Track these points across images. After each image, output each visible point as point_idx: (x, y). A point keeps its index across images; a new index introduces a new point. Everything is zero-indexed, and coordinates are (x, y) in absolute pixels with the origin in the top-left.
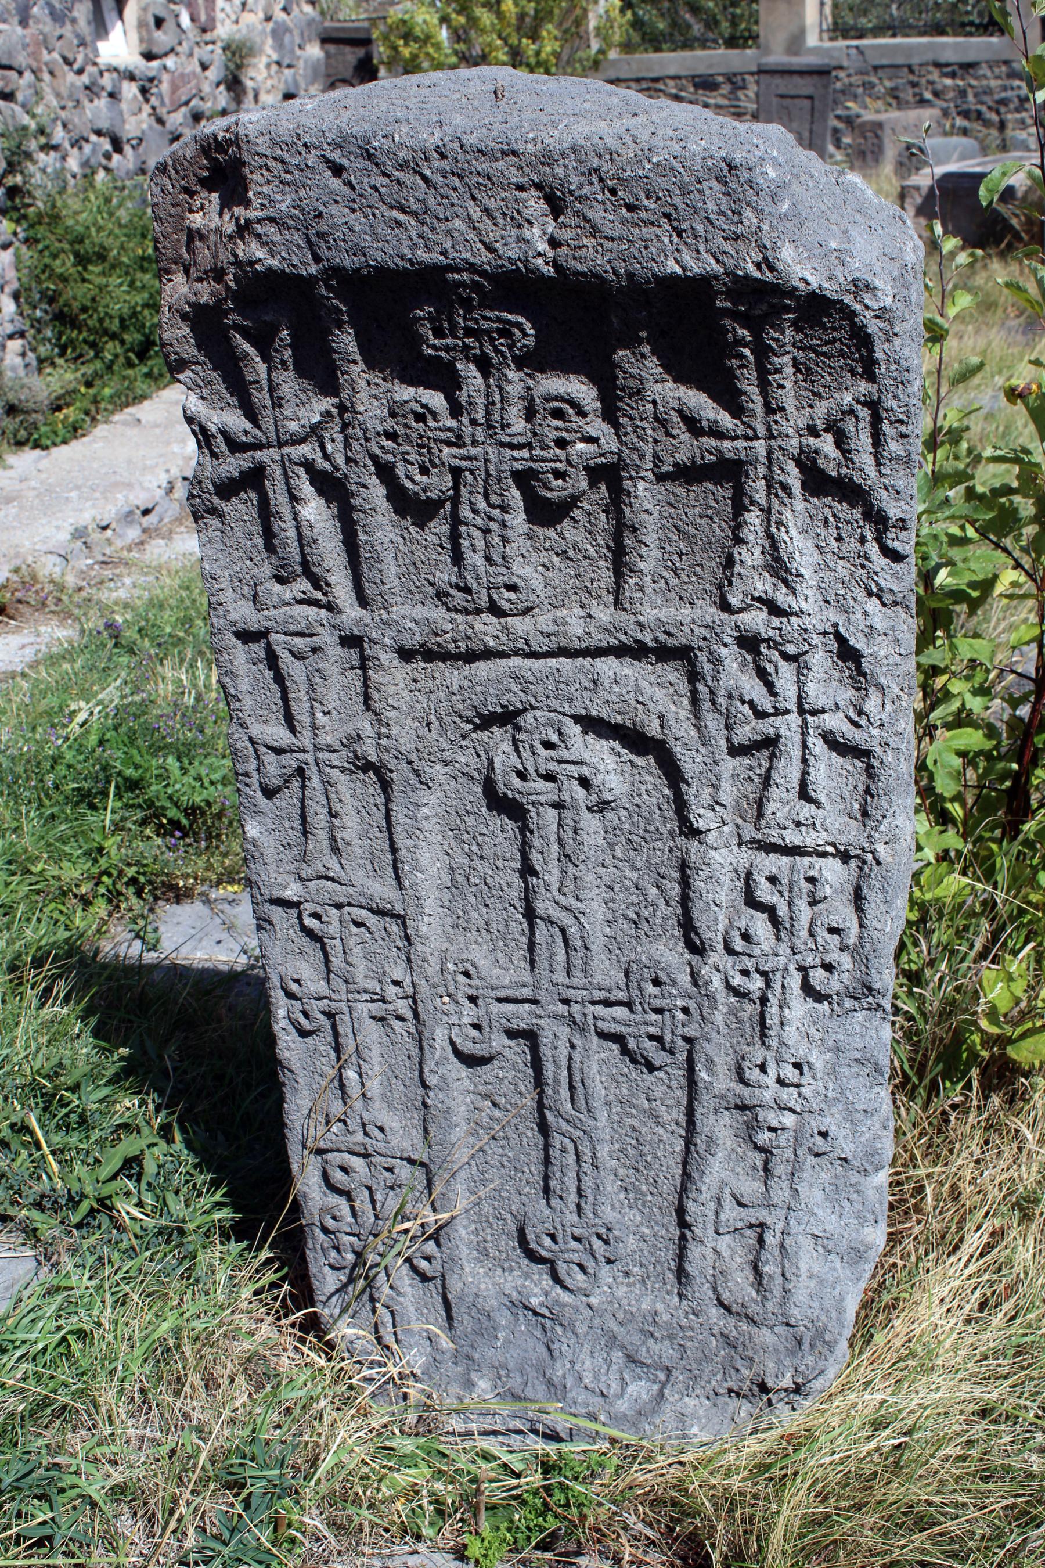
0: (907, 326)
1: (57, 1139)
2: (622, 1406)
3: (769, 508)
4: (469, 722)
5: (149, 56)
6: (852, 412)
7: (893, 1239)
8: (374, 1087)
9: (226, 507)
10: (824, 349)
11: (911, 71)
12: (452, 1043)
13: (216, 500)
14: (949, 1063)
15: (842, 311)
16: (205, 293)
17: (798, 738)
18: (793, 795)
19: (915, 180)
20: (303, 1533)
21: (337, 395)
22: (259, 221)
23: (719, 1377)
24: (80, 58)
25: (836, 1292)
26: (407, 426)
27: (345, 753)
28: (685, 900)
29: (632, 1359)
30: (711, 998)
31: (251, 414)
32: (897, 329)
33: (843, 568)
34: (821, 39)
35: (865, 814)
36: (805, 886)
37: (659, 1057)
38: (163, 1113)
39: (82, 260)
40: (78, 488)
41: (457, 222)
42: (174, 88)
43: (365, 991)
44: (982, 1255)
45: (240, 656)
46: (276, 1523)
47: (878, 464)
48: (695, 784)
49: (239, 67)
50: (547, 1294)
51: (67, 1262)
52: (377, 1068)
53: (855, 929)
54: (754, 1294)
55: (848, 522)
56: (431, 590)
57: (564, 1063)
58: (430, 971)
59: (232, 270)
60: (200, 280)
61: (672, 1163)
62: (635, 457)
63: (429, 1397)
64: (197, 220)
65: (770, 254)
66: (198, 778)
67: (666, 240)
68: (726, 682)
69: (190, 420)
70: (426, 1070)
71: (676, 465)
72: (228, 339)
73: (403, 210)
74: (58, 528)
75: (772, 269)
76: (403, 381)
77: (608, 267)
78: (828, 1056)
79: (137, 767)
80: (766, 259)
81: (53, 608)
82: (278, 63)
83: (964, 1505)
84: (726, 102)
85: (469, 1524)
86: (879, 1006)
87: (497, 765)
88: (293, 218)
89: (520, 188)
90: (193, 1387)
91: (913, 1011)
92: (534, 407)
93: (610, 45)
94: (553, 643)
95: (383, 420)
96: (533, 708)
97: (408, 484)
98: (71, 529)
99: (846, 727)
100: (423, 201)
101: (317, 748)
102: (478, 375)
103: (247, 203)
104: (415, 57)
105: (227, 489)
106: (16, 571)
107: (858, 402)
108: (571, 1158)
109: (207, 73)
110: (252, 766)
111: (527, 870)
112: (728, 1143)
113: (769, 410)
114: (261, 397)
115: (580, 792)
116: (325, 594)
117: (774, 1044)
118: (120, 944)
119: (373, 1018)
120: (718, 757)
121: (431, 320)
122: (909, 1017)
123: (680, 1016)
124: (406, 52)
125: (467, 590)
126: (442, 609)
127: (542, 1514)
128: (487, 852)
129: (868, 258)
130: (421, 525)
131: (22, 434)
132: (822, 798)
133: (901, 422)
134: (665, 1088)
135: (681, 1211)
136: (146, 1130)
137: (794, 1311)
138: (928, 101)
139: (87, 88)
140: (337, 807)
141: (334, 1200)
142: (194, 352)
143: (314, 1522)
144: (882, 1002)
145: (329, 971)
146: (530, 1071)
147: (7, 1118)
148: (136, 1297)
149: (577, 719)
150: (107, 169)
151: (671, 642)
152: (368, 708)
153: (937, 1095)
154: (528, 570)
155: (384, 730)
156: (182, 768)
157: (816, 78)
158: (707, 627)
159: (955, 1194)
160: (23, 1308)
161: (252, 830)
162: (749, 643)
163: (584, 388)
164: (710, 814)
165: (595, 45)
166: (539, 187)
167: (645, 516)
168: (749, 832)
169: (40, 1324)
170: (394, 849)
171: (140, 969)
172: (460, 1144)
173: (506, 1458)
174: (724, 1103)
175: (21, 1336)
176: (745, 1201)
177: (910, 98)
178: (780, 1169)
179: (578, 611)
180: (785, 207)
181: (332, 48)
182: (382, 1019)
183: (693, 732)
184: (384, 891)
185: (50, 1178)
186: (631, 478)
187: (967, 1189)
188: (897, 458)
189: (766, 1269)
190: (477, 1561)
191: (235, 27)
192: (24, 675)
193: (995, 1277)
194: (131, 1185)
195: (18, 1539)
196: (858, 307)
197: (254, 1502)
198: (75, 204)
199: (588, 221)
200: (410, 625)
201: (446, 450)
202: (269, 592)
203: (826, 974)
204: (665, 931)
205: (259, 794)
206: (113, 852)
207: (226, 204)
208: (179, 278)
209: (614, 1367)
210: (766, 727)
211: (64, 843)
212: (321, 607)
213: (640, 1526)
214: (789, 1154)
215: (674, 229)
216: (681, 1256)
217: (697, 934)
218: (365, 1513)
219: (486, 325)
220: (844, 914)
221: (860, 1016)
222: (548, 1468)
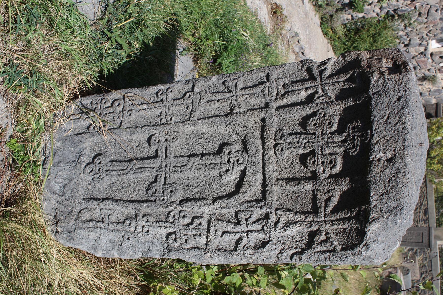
0: (357, 260)
1: (127, 26)
2: (52, 183)
3: (305, 222)
4: (244, 138)
5: (432, 54)
6: (332, 244)
7: (99, 259)
8: (142, 113)
9: (304, 70)
10: (350, 237)
11: (430, 271)
12: (154, 135)
13: (306, 67)
14: (149, 273)
15: (361, 241)
16: (364, 63)
17: (240, 230)
18: (224, 229)
19: (399, 271)
20: (17, 93)
21: (336, 100)
22: (384, 78)
23: (60, 210)
24: (431, 35)
25: (84, 243)
26: (327, 120)
27: (235, 104)
28: (194, 199)
29: (65, 185)
30: (167, 207)
31: (330, 77)
32: (356, 257)
33: (288, 243)
34: (439, 245)
35: (219, 250)
36: (199, 233)
37: (150, 192)
38: (134, 55)
39: (373, 36)
40: (310, 34)
41: (384, 133)
42: (423, 62)
43: (169, 110)
44: (94, 285)
45: (262, 75)
46: (20, 86)
47: (317, 252)
48: (227, 202)
49: (429, 80)
50: (84, 162)
51: (92, 29)
52: (147, 114)
53: (186, 247)
54: (84, 220)
55: (301, 244)
56: (281, 127)
57: (149, 166)
58: (174, 128)
59: (371, 70)
60: (368, 62)
61: (121, 196)
62: (319, 184)
63: (55, 129)
64: (384, 61)
65: (377, 220)
66: (228, 67)
67: (380, 191)
68: (256, 210)
69: (328, 59)
70: (147, 127)
71: (317, 195)
72: (351, 70)
73: (388, 118)
74: (298, 28)
75: (372, 221)
76: (340, 119)
77: (372, 175)
78: (151, 240)
79: (231, 50)
80: (375, 219)
81: (276, 27)
82: (430, 91)
83: (24, 278)
84: (421, 218)
85: (20, 140)
86: (165, 254)
87: (232, 146)
88: (385, 87)
89: (394, 150)
90: (58, 63)
91: (162, 266)
92: (333, 155)
93: (436, 185)
94: (266, 162)
95: (329, 113)
96: (248, 156)
97: (311, 120)
98: (298, 32)
99: (243, 244)
100: (390, 123)
101: (237, 96)
102: (342, 139)
103: (389, 74)
104: (433, 130)
105: (309, 70)
106: (286, 17)
107: (335, 246)
108: (122, 168)
109: (427, 71)
110: (232, 78)
111: (203, 155)
112: (126, 212)
113: (332, 221)
114: (335, 79)
115: (225, 169)
116: (280, 98)
117: (154, 225)
118: (182, 44)
119: (161, 113)
120: (235, 208)
121: (357, 126)
122: (161, 265)
123: (162, 198)
124: (434, 127)
125: (281, 137)
126: (276, 130)
127: (22, 160)
128: (208, 144)
129: (376, 248)
130: (299, 124)
131: (325, 19)
132: (223, 238)
133: (330, 258)
134: (141, 194)
135: (107, 199)
136: (130, 50)
137: (79, 231)
138: (422, 276)
139: (422, 37)
140: (220, 102)
141: (111, 102)
142: (348, 60)
143: (21, 96)
144: (166, 255)
145: (174, 100)
146: (146, 156)
147: (133, 12)
148: (83, 47)
149: (245, 168)
150: (400, 43)
151: (267, 194)
152: (248, 110)
153: (139, 273)
154: (287, 154)
155: (242, 114)
156: (231, 62)
157: (428, 243)
158: (271, 205)
159: (112, 278)
160: (80, 16)
161: (214, 78)
162: (267, 216)
163: (338, 169)
164: (219, 206)
165: (436, 181)
166: (395, 155)
167: (302, 187)
168: (214, 217)
169: (76, 21)
170: (208, 118)
171: (174, 49)
172: (125, 137)
173: (38, 150)
174: (137, 211)
175: (73, 15)
176: (110, 217)
177: (422, 271)
178: (119, 227)
179: (275, 168)
180: (390, 225)
181: (435, 106)
182: (161, 115)
183: (242, 201)
184: (197, 115)
185: (116, 24)
186: (313, 183)
187: (113, 281)
188: (319, 258)
189: (91, 223)
190: (9, 142)
191: (440, 79)
192: (257, 19)
193: (88, 288)
194: (114, 46)
195: (16, 14)
196: (362, 246)
197: (26, 80)
198: (389, 34)
199: (385, 169)
200: (271, 121)
201: (320, 131)
202: (280, 82)
203: (174, 239)
204: (186, 194)
205: (224, 80)
206: (208, 43)
207: (389, 69)
208: (368, 56)
209: (63, 181)
210: (243, 221)
211: (210, 29)
212: (276, 97)
213: (19, 188)
214: (123, 229)
215: (383, 194)
216: (94, 199)
217: (185, 203)
218: (23, 111)
219: (356, 141)
220: (191, 244)
221: (162, 249)
222: (35, 162)
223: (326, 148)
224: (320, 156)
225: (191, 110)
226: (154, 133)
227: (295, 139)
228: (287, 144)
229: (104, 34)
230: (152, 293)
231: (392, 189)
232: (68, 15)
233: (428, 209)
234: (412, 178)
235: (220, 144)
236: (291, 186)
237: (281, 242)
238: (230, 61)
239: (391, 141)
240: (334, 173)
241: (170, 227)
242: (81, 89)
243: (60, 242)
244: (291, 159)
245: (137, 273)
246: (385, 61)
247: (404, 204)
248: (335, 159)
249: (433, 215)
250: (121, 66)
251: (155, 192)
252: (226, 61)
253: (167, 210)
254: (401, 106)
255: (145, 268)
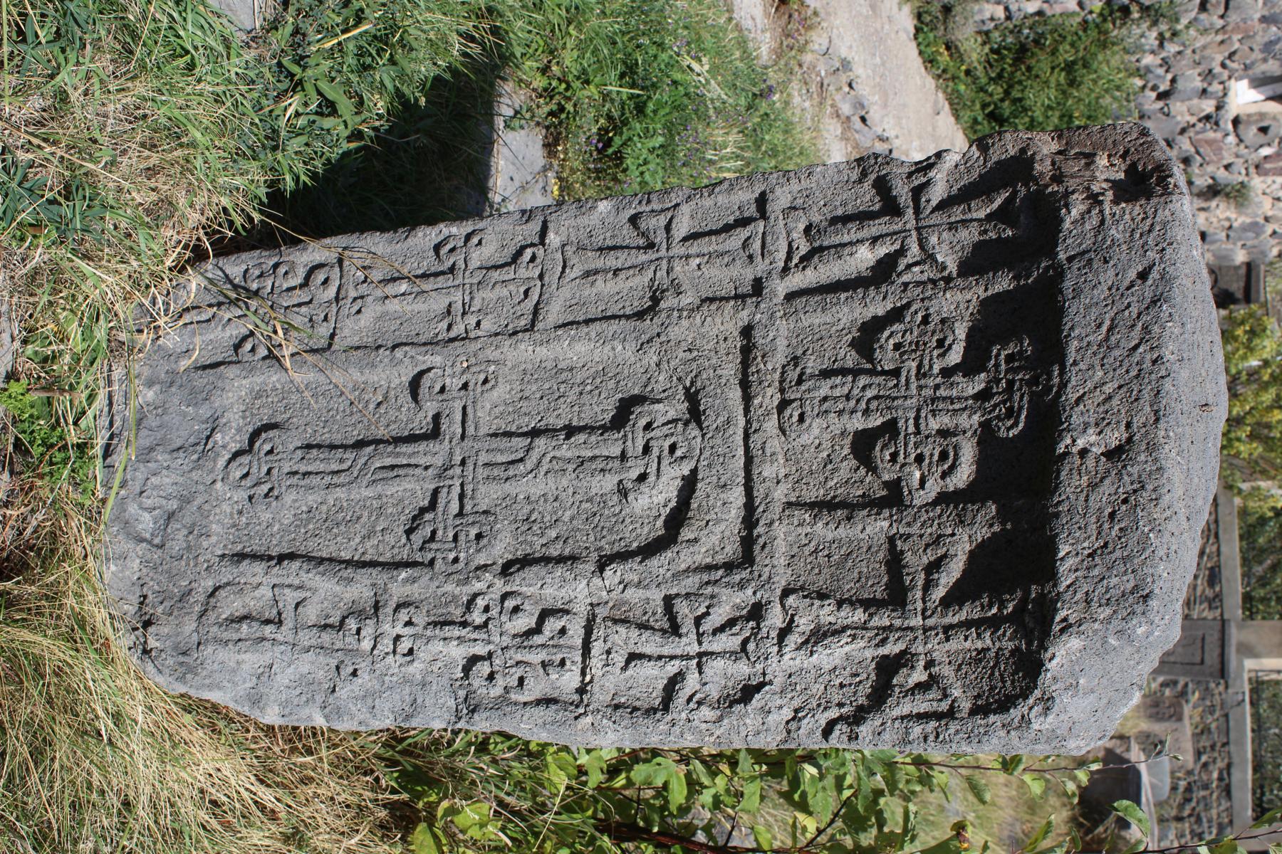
0: (1016, 742)
1: (351, 46)
2: (133, 509)
3: (866, 629)
4: (692, 383)
5: (1236, 122)
6: (945, 696)
7: (269, 730)
8: (394, 306)
10: (997, 674)
11: (1224, 745)
12: (429, 370)
13: (873, 176)
14: (412, 776)
15: (1028, 688)
16: (1043, 168)
17: (679, 652)
18: (632, 648)
20: (29, 248)
21: (959, 275)
22: (1101, 211)
23: (156, 588)
25: (225, 683)
26: (934, 332)
27: (666, 282)
28: (546, 560)
29: (171, 516)
30: (466, 581)
31: (943, 205)
32: (1013, 733)
33: (817, 689)
34: (1250, 671)
35: (617, 707)
36: (558, 658)
37: (417, 538)
38: (372, 133)
39: (1069, 67)
40: (883, 64)
41: (1100, 374)
42: (1210, 143)
43: (472, 299)
45: (745, 197)
46: (37, 226)
47: (903, 718)
48: (641, 568)
49: (1227, 195)
50: (224, 447)
51: (250, 55)
52: (409, 308)
54: (224, 616)
55: (855, 693)
56: (799, 353)
57: (413, 461)
58: (488, 352)
59: (1062, 189)
60: (1053, 163)
61: (331, 549)
62: (909, 519)
64: (1102, 161)
65: (1074, 629)
66: (646, 162)
67: (1086, 544)
68: (724, 593)
69: (939, 155)
70: (407, 348)
71: (902, 552)
72: (1005, 187)
73: (1110, 329)
74: (851, 47)
75: (1062, 631)
77: (1063, 497)
78: (419, 677)
79: (655, 112)
80: (1070, 626)
81: (785, 43)
82: (1230, 227)
83: (52, 788)
84: (1198, 593)
86: (460, 718)
87: (656, 406)
89: (1128, 425)
90: (149, 157)
92: (950, 437)
93: (1245, 498)
95: (939, 313)
96: (703, 436)
97: (886, 333)
98: (849, 58)
99: (687, 692)
100: (1117, 346)
101: (670, 259)
102: (975, 391)
103: (1116, 202)
104: (1236, 339)
105: (882, 186)
106: (816, 13)
107: (953, 701)
108: (335, 467)
109: (1222, 169)
110: (656, 205)
111: (570, 431)
112: (348, 595)
113: (947, 629)
114: (957, 213)
115: (634, 474)
116: (796, 266)
117: (429, 633)
118: (510, 98)
120: (663, 586)
121: (1021, 352)
123: (452, 556)
124: (1239, 332)
125: (800, 381)
126: (784, 361)
127: (44, 443)
128: (586, 398)
129: (1071, 709)
130: (852, 344)
131: (927, 18)
132: (630, 672)
133: (937, 737)
134: (393, 544)
135: (292, 556)
136: (358, 119)
137: (210, 649)
138: (1199, 759)
139: (1210, 71)
140: (622, 275)
141: (301, 273)
142: (995, 159)
143: (38, 257)
144: (463, 721)
145: (488, 269)
146: (406, 433)
147: (368, 5)
149: (694, 472)
150: (1144, 87)
151: (757, 548)
153: (386, 766)
154: (816, 431)
155: (685, 313)
156: (654, 148)
157: (1218, 666)
158: (770, 578)
159: (305, 781)
160: (213, 19)
161: (604, 206)
162: (757, 612)
163: (965, 477)
165: (1245, 486)
166: (1130, 440)
167: (860, 527)
168: (602, 612)
169: (199, 33)
170: (587, 322)
172: (346, 376)
173: (90, 413)
174: (380, 592)
175: (190, 17)
176: (300, 609)
177: (1201, 744)
178: (326, 637)
179: (782, 472)
180: (1113, 641)
181: (1243, 271)
183: (683, 566)
184: (554, 313)
185: (319, 41)
186: (891, 516)
187: (310, 790)
188: (907, 733)
189: (245, 626)
190: (6, 390)
191: (1260, 192)
192: (730, 19)
193: (238, 813)
194: (313, 107)
195: (24, 15)
196: (1031, 701)
197: (54, 208)
198: (1115, 61)
199: (1101, 481)
200: (771, 335)
201: (914, 365)
202: (798, 220)
204: (521, 543)
205: (633, 212)
206: (586, 93)
207: (1115, 184)
208: (1055, 146)
209: (164, 502)
210: (687, 626)
212: (786, 262)
213: (34, 523)
214: (339, 645)
215: (1095, 551)
216: (255, 557)
217: (518, 570)
218: (45, 298)
219: (1017, 397)
221: (452, 703)
222: (82, 447)
223: (929, 416)
224: (913, 439)
225: (536, 298)
226: (429, 365)
227: (839, 389)
228: (816, 401)
229: (281, 72)
230: (425, 825)
231: (1120, 538)
232: (175, 15)
233: (1219, 567)
234: (1180, 508)
235: (621, 400)
236: (827, 524)
237: (798, 688)
238: (651, 145)
239: (1118, 397)
240: (952, 489)
241: (475, 640)
242: (215, 232)
243: (157, 680)
244: (827, 445)
245: (380, 768)
246: (1105, 162)
247: (1153, 582)
248: (956, 448)
249: (1234, 585)
250: (334, 166)
251: (433, 538)
252: (639, 145)
253: (465, 592)
254: (1148, 295)
255: (404, 752)
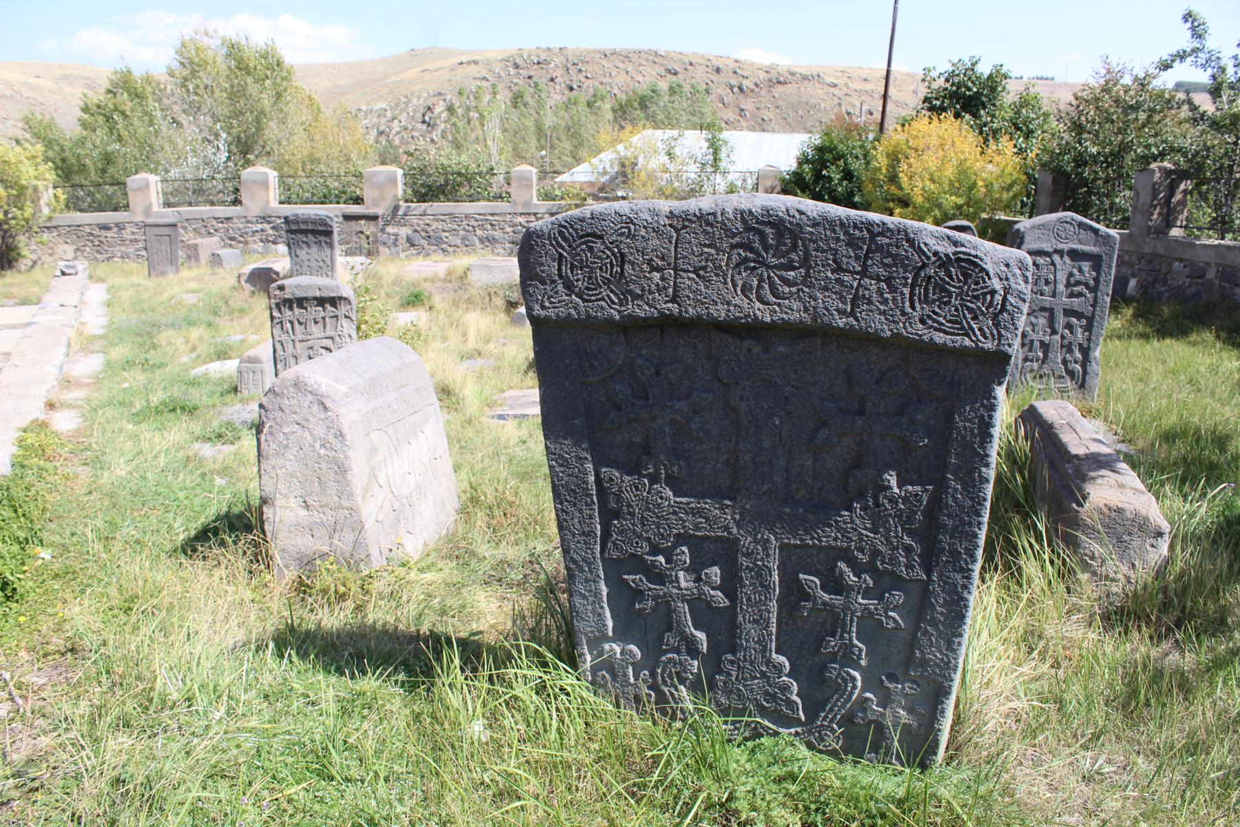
92: (316, 311)
